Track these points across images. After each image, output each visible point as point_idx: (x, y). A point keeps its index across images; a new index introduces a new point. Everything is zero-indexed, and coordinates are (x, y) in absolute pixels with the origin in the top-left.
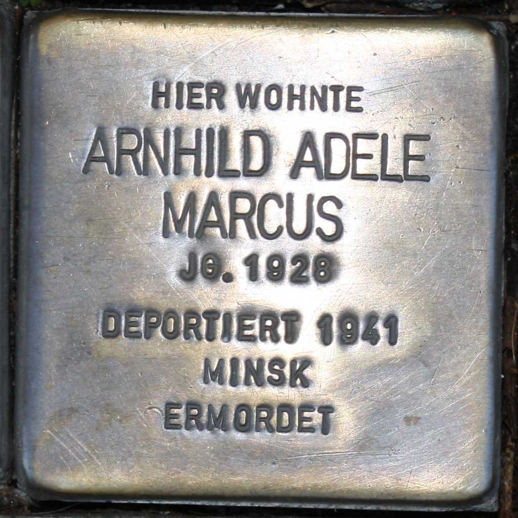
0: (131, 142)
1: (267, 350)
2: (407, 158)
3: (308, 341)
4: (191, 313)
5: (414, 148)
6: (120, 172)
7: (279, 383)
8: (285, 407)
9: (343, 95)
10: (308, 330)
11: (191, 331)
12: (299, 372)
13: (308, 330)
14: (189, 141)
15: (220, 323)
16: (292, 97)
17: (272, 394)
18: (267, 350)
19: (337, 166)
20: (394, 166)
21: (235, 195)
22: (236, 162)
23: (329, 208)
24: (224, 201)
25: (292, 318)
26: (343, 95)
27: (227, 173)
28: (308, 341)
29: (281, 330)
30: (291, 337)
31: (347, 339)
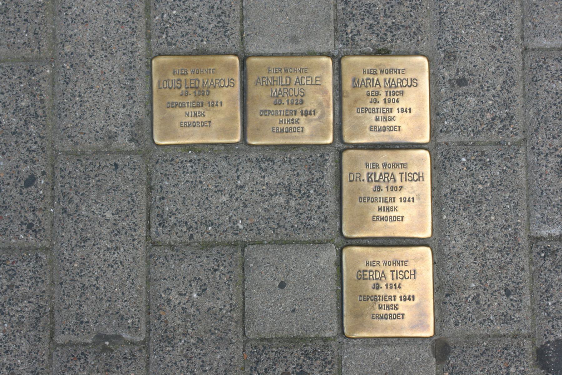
0: (264, 80)
1: (390, 303)
2: (316, 81)
3: (398, 301)
4: (376, 296)
5: (318, 79)
6: (263, 85)
7: (293, 123)
8: (395, 314)
9: (404, 263)
10: (398, 299)
11: (277, 115)
12: (297, 121)
13: (398, 299)
14: (275, 79)
15: (282, 112)
16: (393, 263)
17: (293, 126)
18: (390, 303)
19: (303, 83)
20: (314, 83)
21: (284, 89)
22: (284, 83)
23: (302, 91)
24: (282, 90)
25: (296, 111)
26: (404, 263)
27: (282, 85)
28: (398, 301)
29: (294, 113)
30: (395, 300)
31: (405, 300)
